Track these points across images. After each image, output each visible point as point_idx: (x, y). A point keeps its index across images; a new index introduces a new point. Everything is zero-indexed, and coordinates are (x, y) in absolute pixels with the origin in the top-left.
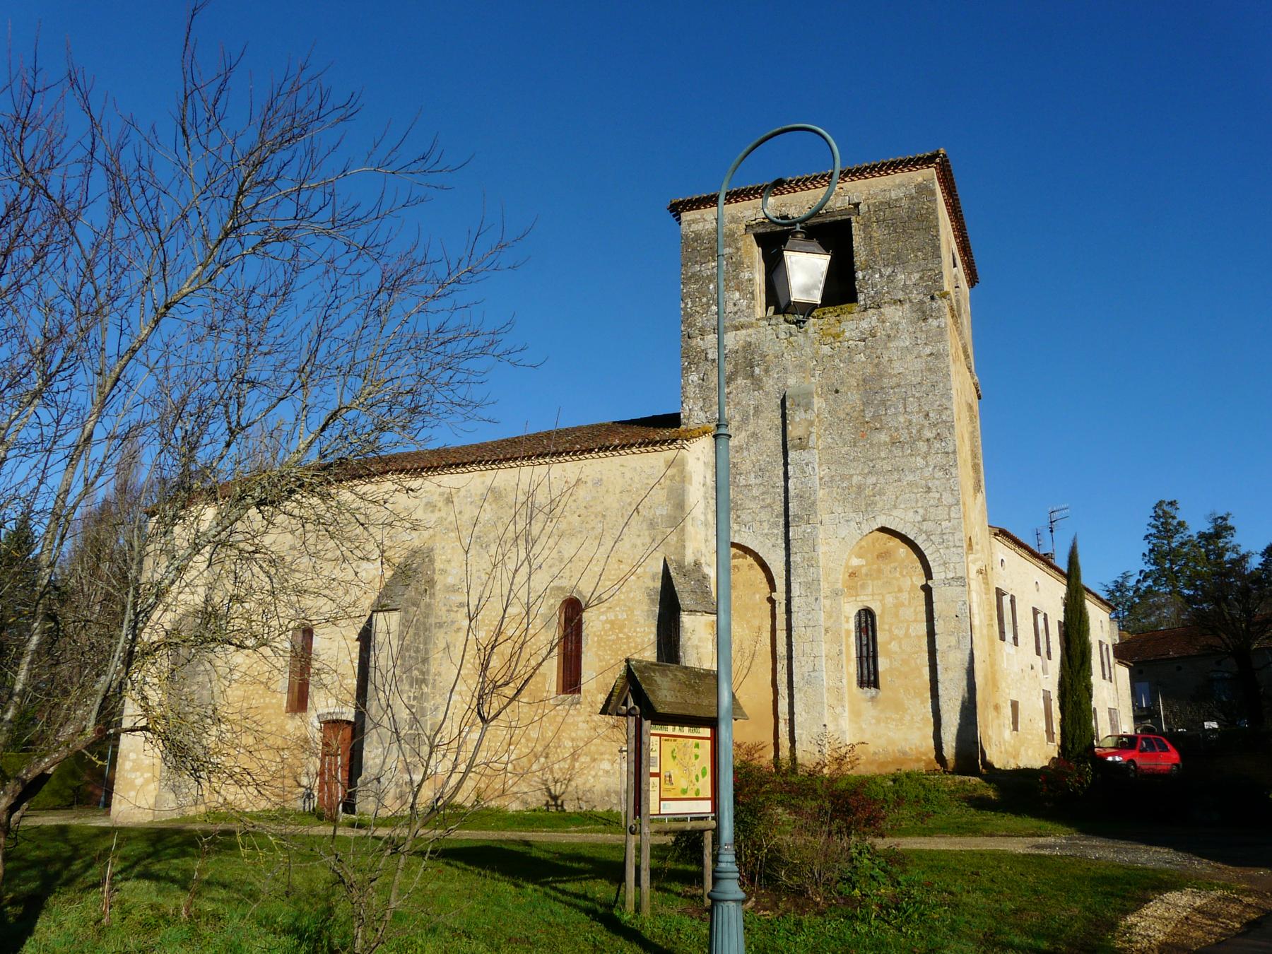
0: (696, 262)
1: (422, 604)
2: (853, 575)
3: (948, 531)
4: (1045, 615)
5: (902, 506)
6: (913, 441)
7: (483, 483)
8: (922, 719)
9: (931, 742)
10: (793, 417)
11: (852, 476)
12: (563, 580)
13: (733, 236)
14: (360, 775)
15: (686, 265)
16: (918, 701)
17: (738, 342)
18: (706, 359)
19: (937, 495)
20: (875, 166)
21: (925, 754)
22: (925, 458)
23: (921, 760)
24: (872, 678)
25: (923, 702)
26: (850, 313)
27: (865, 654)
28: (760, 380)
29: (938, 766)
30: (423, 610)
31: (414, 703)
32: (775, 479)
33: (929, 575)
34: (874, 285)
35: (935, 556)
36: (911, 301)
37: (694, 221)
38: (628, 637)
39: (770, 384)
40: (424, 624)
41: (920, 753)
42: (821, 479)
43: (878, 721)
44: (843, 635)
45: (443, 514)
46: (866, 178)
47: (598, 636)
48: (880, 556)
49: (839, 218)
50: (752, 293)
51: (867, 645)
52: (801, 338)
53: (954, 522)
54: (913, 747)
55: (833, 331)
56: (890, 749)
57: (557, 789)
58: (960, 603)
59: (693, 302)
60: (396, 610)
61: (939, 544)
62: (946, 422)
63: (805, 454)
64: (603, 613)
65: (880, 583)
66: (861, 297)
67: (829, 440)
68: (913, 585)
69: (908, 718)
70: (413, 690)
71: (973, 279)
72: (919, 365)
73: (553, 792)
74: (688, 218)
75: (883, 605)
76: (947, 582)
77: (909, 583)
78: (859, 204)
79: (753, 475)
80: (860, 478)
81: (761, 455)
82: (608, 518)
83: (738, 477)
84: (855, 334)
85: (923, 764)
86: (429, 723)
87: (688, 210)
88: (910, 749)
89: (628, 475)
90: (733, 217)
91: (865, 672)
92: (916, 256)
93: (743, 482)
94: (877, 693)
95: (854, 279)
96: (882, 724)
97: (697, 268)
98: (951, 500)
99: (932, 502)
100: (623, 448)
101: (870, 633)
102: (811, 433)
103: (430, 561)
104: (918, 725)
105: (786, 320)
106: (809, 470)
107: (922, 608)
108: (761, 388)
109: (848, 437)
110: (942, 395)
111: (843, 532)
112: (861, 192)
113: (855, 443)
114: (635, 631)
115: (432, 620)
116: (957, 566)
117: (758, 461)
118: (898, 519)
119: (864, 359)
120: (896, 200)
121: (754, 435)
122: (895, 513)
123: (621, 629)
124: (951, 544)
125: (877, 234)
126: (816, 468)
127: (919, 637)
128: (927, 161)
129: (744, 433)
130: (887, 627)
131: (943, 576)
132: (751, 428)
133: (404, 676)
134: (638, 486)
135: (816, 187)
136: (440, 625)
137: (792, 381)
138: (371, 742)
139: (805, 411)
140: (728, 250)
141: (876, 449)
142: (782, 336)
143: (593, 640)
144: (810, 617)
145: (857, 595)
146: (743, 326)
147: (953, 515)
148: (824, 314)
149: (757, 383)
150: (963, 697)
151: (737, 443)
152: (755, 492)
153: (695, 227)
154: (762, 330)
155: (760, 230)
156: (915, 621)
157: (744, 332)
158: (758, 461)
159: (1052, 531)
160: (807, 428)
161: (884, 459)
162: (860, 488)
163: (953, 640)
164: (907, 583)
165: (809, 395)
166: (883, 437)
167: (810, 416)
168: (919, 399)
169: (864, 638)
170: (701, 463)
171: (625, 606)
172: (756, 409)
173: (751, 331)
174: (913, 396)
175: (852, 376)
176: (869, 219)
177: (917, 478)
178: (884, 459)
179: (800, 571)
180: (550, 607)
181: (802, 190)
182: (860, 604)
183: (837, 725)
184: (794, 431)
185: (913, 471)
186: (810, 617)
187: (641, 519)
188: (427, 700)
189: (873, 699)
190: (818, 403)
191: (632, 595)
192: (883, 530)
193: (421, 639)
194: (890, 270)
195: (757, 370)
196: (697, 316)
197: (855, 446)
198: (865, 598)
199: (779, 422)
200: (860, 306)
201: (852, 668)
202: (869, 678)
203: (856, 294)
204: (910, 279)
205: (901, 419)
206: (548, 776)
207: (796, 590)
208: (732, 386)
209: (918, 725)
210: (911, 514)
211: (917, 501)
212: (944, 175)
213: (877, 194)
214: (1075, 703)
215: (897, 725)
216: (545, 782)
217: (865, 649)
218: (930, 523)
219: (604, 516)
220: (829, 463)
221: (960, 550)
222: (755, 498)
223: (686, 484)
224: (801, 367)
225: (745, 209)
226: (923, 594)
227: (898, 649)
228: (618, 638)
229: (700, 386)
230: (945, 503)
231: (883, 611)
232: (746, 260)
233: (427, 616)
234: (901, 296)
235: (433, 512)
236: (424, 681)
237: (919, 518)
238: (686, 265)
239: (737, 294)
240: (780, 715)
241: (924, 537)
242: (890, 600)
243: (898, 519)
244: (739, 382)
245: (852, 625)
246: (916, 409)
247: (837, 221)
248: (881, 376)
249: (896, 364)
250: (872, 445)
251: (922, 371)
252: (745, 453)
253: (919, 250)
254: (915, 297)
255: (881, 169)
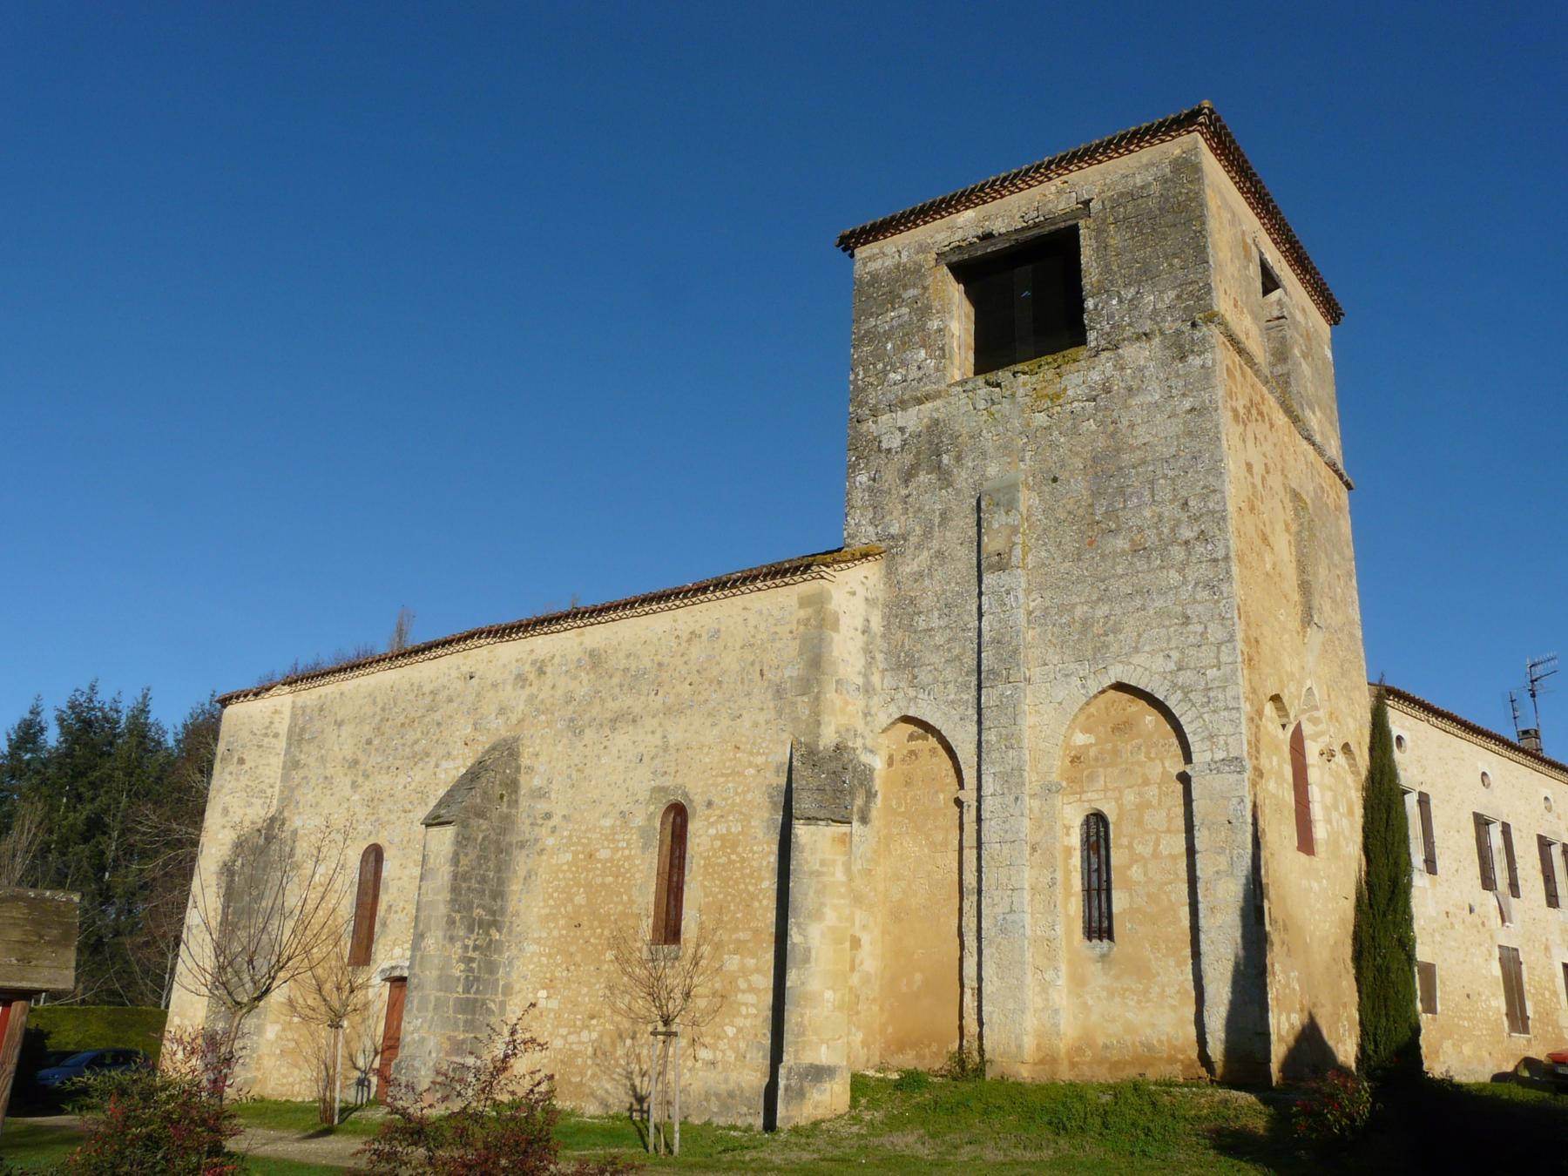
0: (871, 315)
1: (495, 814)
2: (1075, 760)
3: (1217, 684)
4: (1506, 830)
5: (1147, 648)
6: (1164, 547)
7: (581, 644)
8: (1178, 992)
9: (1192, 1031)
10: (990, 523)
11: (1074, 606)
12: (667, 777)
13: (919, 271)
14: (781, 1061)
15: (858, 321)
16: (1172, 962)
17: (922, 420)
18: (880, 450)
19: (1200, 628)
20: (1110, 142)
21: (1183, 1051)
22: (1181, 571)
23: (1177, 1060)
24: (1105, 924)
25: (1179, 964)
26: (1075, 361)
27: (1095, 885)
28: (950, 473)
29: (1203, 1072)
30: (496, 824)
31: (475, 955)
32: (966, 618)
33: (1188, 757)
34: (1111, 316)
35: (1195, 725)
36: (1162, 333)
37: (871, 258)
38: (743, 860)
39: (962, 478)
40: (498, 842)
41: (1175, 1047)
42: (1030, 613)
43: (1111, 994)
44: (1060, 856)
45: (534, 690)
46: (1100, 162)
47: (705, 858)
48: (1116, 729)
49: (1062, 225)
50: (942, 349)
51: (1099, 870)
52: (1006, 406)
53: (1226, 669)
54: (1164, 1038)
55: (1050, 391)
56: (1129, 1039)
57: (644, 1086)
58: (1235, 801)
59: (866, 371)
60: (449, 823)
61: (1202, 706)
62: (1213, 512)
63: (1005, 576)
64: (712, 824)
65: (1117, 772)
66: (1091, 336)
67: (1043, 554)
68: (1165, 773)
69: (1155, 990)
70: (473, 937)
71: (1332, 311)
72: (1174, 427)
73: (638, 1090)
74: (864, 255)
75: (1120, 807)
76: (1214, 767)
77: (1160, 770)
78: (1090, 200)
79: (936, 613)
80: (1085, 608)
81: (948, 583)
82: (725, 686)
83: (916, 618)
84: (1082, 391)
85: (1179, 1067)
86: (501, 983)
87: (863, 244)
88: (1160, 1041)
89: (752, 622)
90: (920, 246)
91: (1095, 914)
92: (1171, 265)
93: (923, 625)
94: (1110, 949)
95: (1082, 310)
96: (1118, 999)
97: (872, 321)
98: (1221, 635)
99: (1192, 639)
100: (743, 583)
101: (1103, 852)
102: (1015, 544)
103: (510, 755)
104: (1171, 1001)
105: (988, 383)
106: (1010, 600)
107: (1180, 810)
108: (950, 485)
109: (1070, 547)
110: (1208, 471)
111: (1060, 694)
112: (1093, 183)
113: (1079, 554)
114: (751, 851)
115: (514, 838)
116: (1230, 740)
117: (944, 591)
118: (1139, 669)
119: (1094, 427)
120: (1142, 188)
121: (939, 554)
122: (1136, 659)
123: (735, 845)
124: (1221, 705)
125: (1116, 239)
126: (1021, 595)
127: (1173, 857)
128: (1184, 123)
129: (926, 553)
130: (1125, 841)
131: (1208, 756)
132: (935, 545)
133: (458, 917)
134: (765, 636)
135: (1031, 186)
136: (522, 845)
137: (992, 470)
138: (411, 1009)
139: (1007, 513)
140: (912, 292)
141: (1109, 563)
142: (982, 405)
143: (698, 865)
144: (1007, 826)
145: (1083, 792)
146: (928, 398)
147: (1224, 658)
148: (1039, 367)
149: (945, 478)
150: (1236, 956)
151: (916, 568)
152: (939, 639)
153: (872, 266)
154: (952, 400)
155: (955, 258)
156: (1168, 831)
157: (929, 405)
158: (944, 591)
159: (1533, 695)
160: (1009, 537)
161: (1121, 576)
162: (1086, 624)
163: (1223, 862)
164: (1155, 771)
165: (1012, 488)
166: (1121, 543)
167: (1013, 519)
168: (1173, 479)
169: (1094, 860)
170: (859, 601)
171: (741, 813)
172: (943, 515)
173: (939, 403)
174: (1165, 477)
175: (1077, 454)
176: (1104, 220)
177: (1169, 603)
178: (1121, 576)
179: (995, 755)
180: (649, 818)
181: (1012, 192)
182: (1086, 805)
183: (1047, 1000)
184: (991, 544)
185: (1162, 593)
186: (1007, 826)
187: (766, 684)
188: (499, 951)
189: (1103, 957)
190: (1027, 499)
191: (749, 797)
192: (1120, 687)
193: (491, 865)
194: (1133, 290)
195: (945, 459)
196: (870, 389)
197: (1079, 560)
198: (1094, 796)
199: (973, 532)
200: (1091, 349)
201: (1074, 907)
202: (1099, 926)
203: (1085, 332)
204: (1163, 300)
205: (1147, 513)
206: (635, 1067)
207: (987, 789)
208: (912, 485)
209: (1171, 1001)
210: (1160, 659)
211: (1169, 639)
212: (1220, 142)
213: (1115, 183)
214: (1379, 969)
215: (1139, 1002)
216: (629, 1076)
217: (1094, 876)
218: (1189, 672)
219: (720, 683)
220: (1041, 587)
221: (1234, 714)
222: (937, 647)
223: (828, 633)
224: (1006, 449)
225: (937, 232)
226: (1180, 787)
227: (1142, 878)
228: (731, 862)
229: (870, 489)
230: (1212, 639)
231: (1120, 817)
232: (936, 304)
233: (503, 832)
234: (1147, 326)
235: (523, 687)
236: (495, 924)
237: (1172, 666)
238: (858, 321)
239: (923, 353)
240: (966, 981)
241: (1179, 694)
242: (1130, 797)
243: (1139, 669)
244: (922, 478)
245: (1075, 839)
246: (1169, 496)
247: (1059, 230)
248: (1118, 450)
249: (1140, 430)
250: (1103, 557)
251: (1178, 437)
252: (927, 582)
253: (1175, 255)
254: (1169, 326)
255: (1118, 145)
